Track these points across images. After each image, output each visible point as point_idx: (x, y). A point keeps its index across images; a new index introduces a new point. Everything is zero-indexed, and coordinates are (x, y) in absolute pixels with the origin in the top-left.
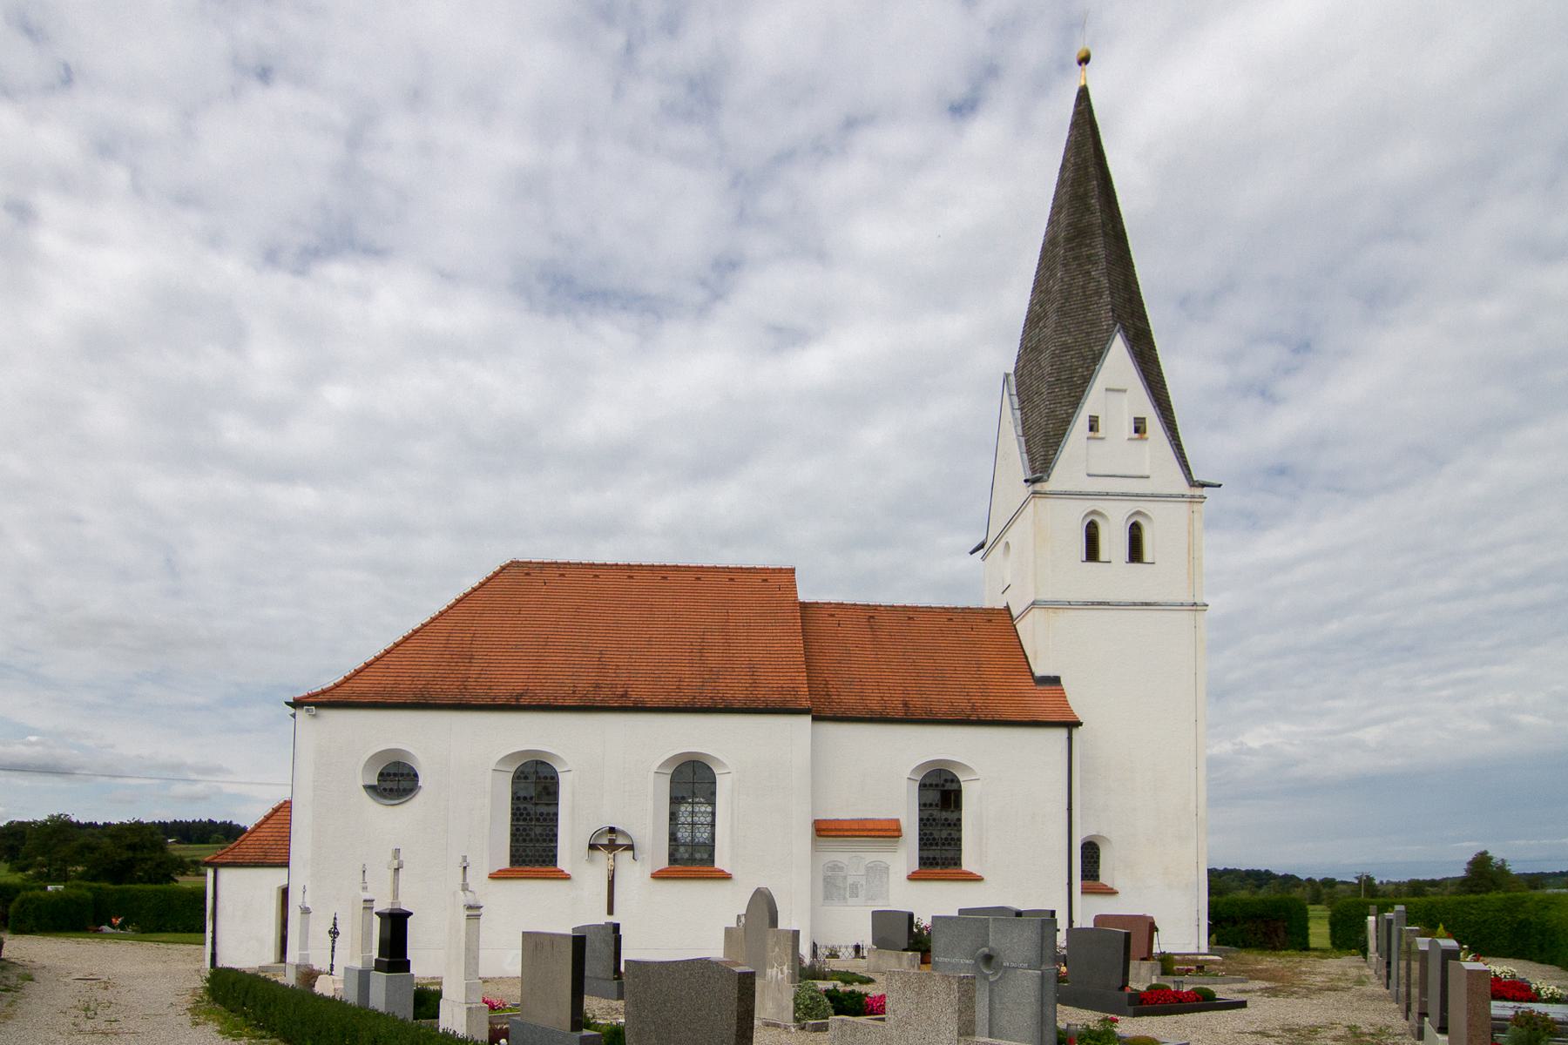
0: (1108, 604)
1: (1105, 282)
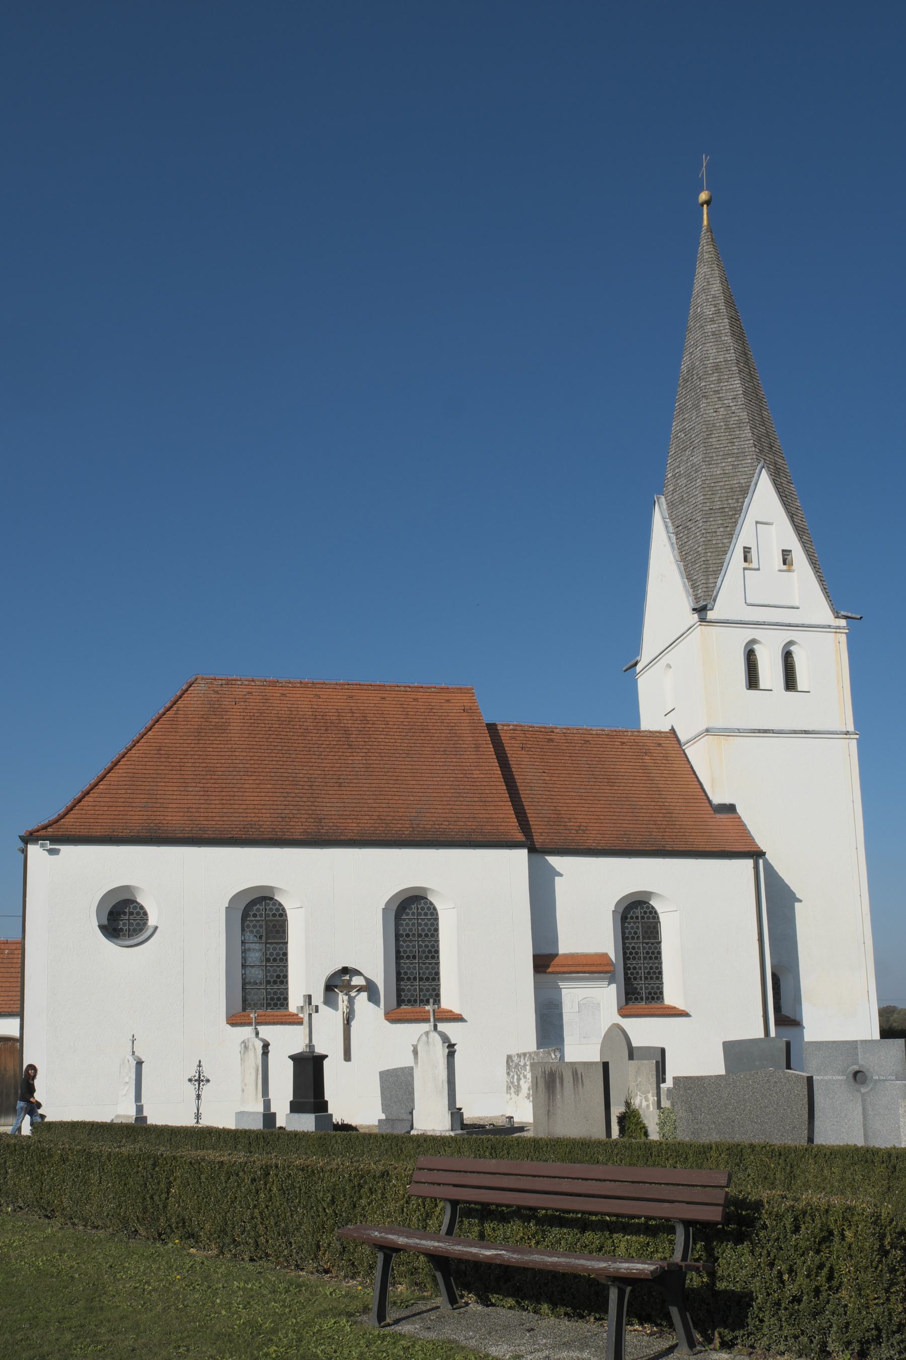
0: (773, 731)
1: (744, 415)
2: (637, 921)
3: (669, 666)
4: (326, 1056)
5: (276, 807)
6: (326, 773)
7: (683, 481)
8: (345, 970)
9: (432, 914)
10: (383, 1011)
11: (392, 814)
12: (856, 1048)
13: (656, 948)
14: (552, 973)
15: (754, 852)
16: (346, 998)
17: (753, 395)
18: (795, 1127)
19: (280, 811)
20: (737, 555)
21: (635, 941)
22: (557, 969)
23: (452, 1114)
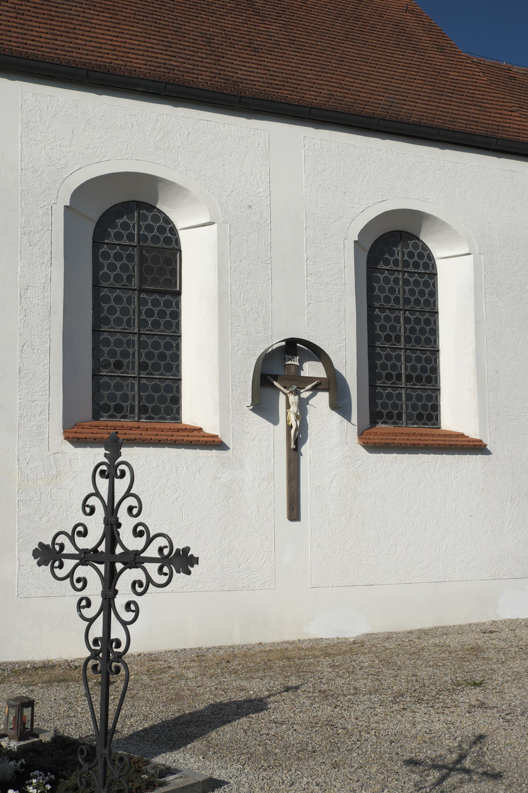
8: (292, 346)
10: (356, 429)
16: (293, 399)
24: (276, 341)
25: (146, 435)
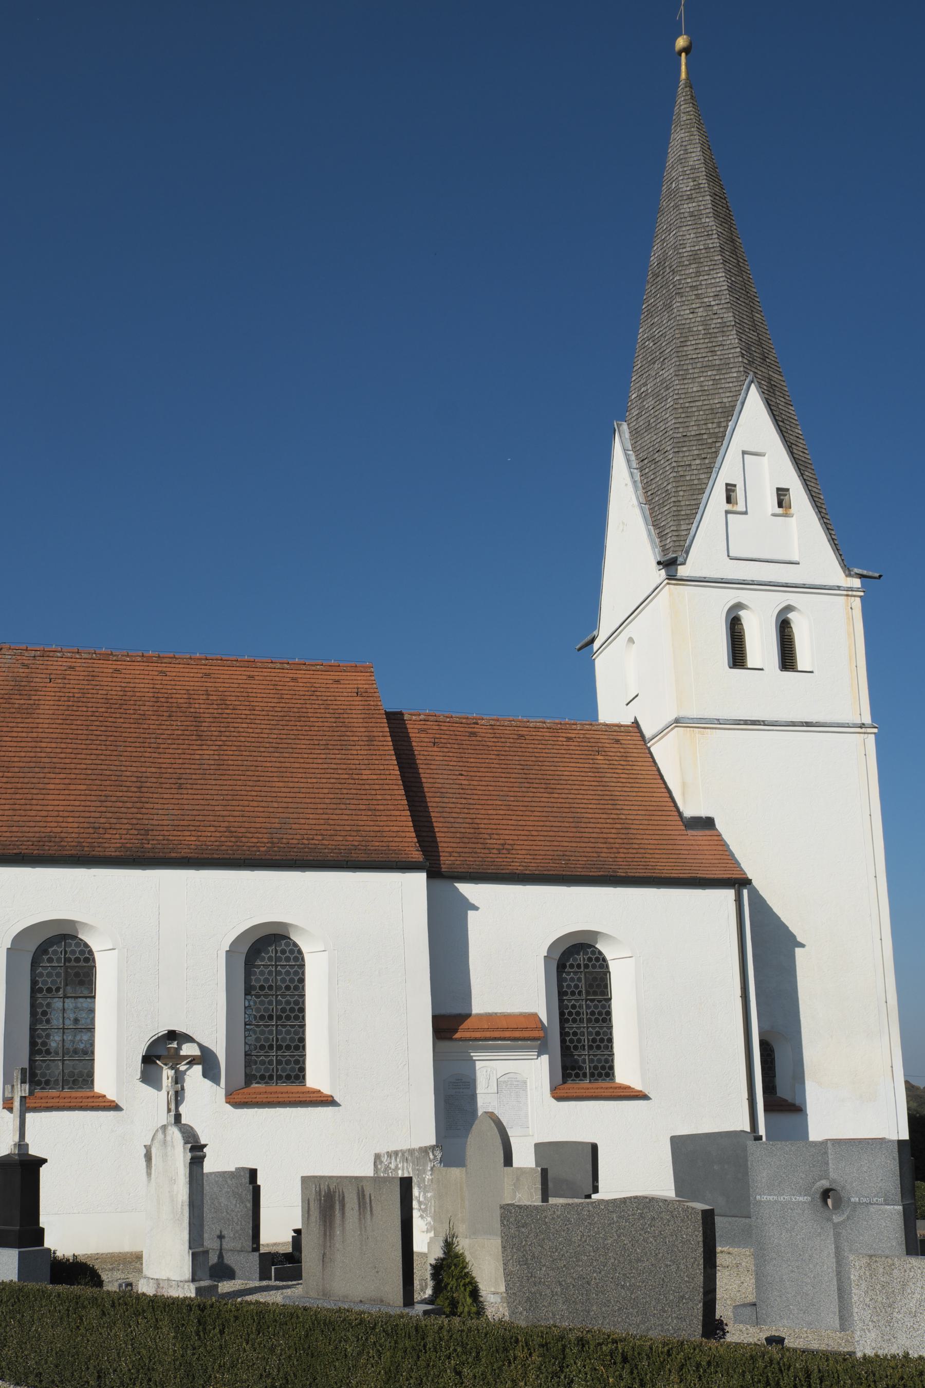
0: (764, 723)
1: (729, 317)
2: (579, 971)
3: (631, 640)
4: (44, 1161)
5: (88, 814)
6: (163, 770)
7: (649, 403)
8: (172, 1035)
9: (296, 959)
11: (246, 825)
12: (826, 1153)
13: (604, 1007)
14: (461, 1039)
15: (736, 879)
16: (171, 1073)
17: (742, 292)
18: (683, 1297)
19: (92, 820)
20: (718, 494)
21: (576, 997)
22: (467, 1035)
23: (193, 1254)
24: (163, 1030)
25: (62, 1103)
